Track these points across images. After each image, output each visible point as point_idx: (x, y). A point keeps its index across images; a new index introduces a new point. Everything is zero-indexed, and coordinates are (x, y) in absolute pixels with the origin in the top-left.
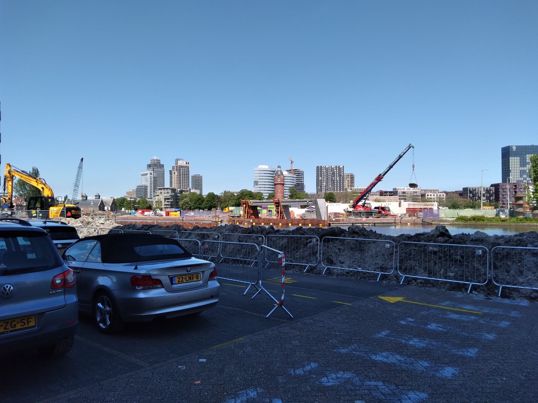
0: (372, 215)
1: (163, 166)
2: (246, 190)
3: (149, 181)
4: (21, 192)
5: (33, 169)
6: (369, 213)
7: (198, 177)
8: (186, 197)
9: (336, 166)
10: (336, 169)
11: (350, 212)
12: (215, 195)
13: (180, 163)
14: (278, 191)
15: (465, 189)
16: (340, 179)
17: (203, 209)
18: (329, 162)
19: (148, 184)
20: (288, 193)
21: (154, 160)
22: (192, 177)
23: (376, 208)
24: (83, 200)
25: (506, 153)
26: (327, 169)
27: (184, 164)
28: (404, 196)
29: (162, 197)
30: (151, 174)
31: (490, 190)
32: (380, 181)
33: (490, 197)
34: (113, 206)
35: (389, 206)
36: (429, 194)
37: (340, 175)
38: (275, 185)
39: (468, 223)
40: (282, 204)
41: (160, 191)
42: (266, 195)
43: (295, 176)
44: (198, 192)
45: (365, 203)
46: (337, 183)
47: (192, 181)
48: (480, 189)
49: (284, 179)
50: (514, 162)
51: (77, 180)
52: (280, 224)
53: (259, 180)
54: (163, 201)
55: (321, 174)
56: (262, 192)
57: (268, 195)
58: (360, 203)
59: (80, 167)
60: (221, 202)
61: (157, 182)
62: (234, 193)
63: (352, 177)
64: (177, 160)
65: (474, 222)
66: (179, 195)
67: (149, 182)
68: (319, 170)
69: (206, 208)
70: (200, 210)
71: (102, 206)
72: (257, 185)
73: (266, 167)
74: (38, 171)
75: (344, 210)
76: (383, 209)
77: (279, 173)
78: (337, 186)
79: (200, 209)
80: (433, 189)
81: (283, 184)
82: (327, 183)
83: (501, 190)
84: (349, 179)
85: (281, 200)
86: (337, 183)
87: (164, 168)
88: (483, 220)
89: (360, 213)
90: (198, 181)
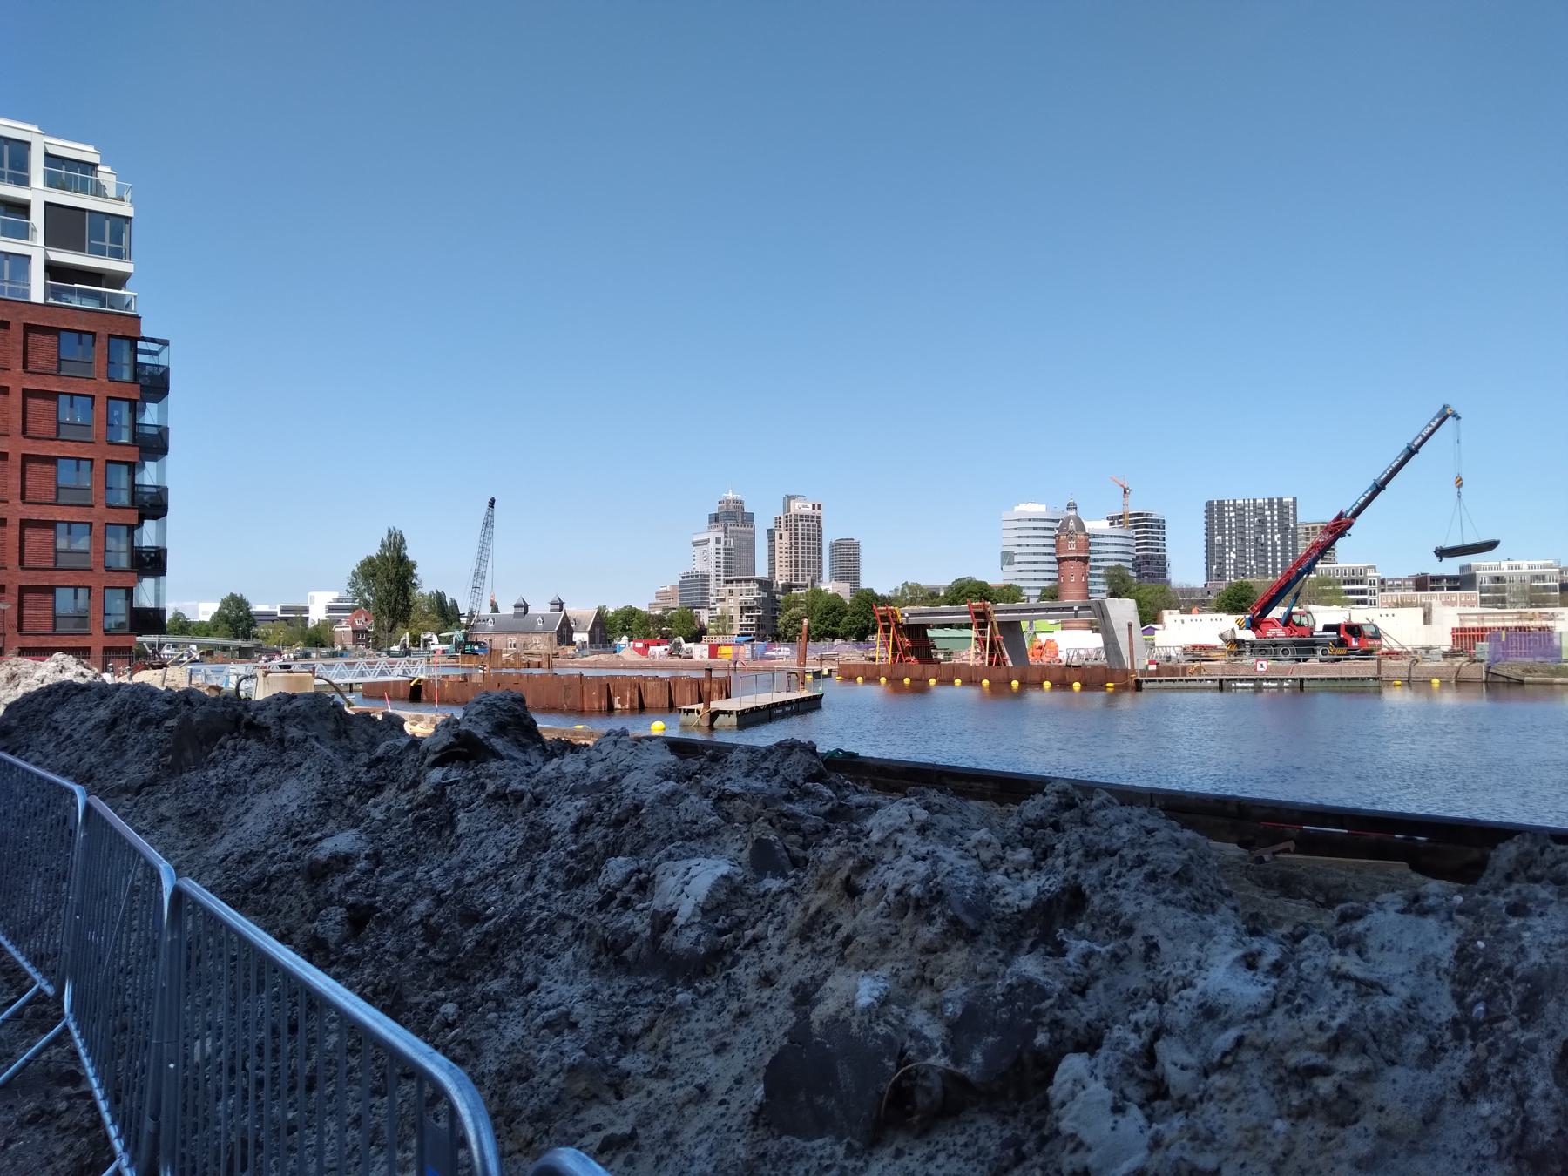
1: (750, 517)
2: (970, 581)
3: (713, 560)
5: (390, 535)
6: (1305, 647)
9: (1271, 501)
10: (1271, 509)
11: (1240, 643)
13: (797, 507)
16: (1284, 540)
17: (844, 638)
18: (1246, 488)
19: (712, 570)
20: (1101, 588)
22: (833, 546)
23: (1327, 628)
24: (516, 615)
26: (1239, 510)
27: (809, 510)
28: (1497, 590)
30: (718, 540)
32: (1342, 534)
34: (598, 630)
35: (1383, 625)
37: (1284, 529)
38: (1060, 561)
40: (996, 617)
42: (1032, 594)
43: (1132, 533)
45: (1290, 615)
46: (1274, 551)
47: (833, 559)
51: (482, 560)
52: (907, 681)
53: (1017, 550)
54: (736, 614)
55: (1221, 523)
56: (1019, 584)
57: (1038, 592)
58: (1278, 612)
59: (488, 524)
61: (735, 564)
62: (938, 589)
64: (788, 499)
68: (1215, 513)
70: (837, 642)
71: (565, 633)
72: (1011, 563)
73: (1038, 509)
74: (403, 541)
75: (1221, 636)
76: (1354, 630)
77: (1072, 524)
79: (834, 636)
81: (1085, 560)
82: (1241, 553)
86: (1274, 551)
87: (756, 522)
89: (1275, 645)
90: (847, 558)
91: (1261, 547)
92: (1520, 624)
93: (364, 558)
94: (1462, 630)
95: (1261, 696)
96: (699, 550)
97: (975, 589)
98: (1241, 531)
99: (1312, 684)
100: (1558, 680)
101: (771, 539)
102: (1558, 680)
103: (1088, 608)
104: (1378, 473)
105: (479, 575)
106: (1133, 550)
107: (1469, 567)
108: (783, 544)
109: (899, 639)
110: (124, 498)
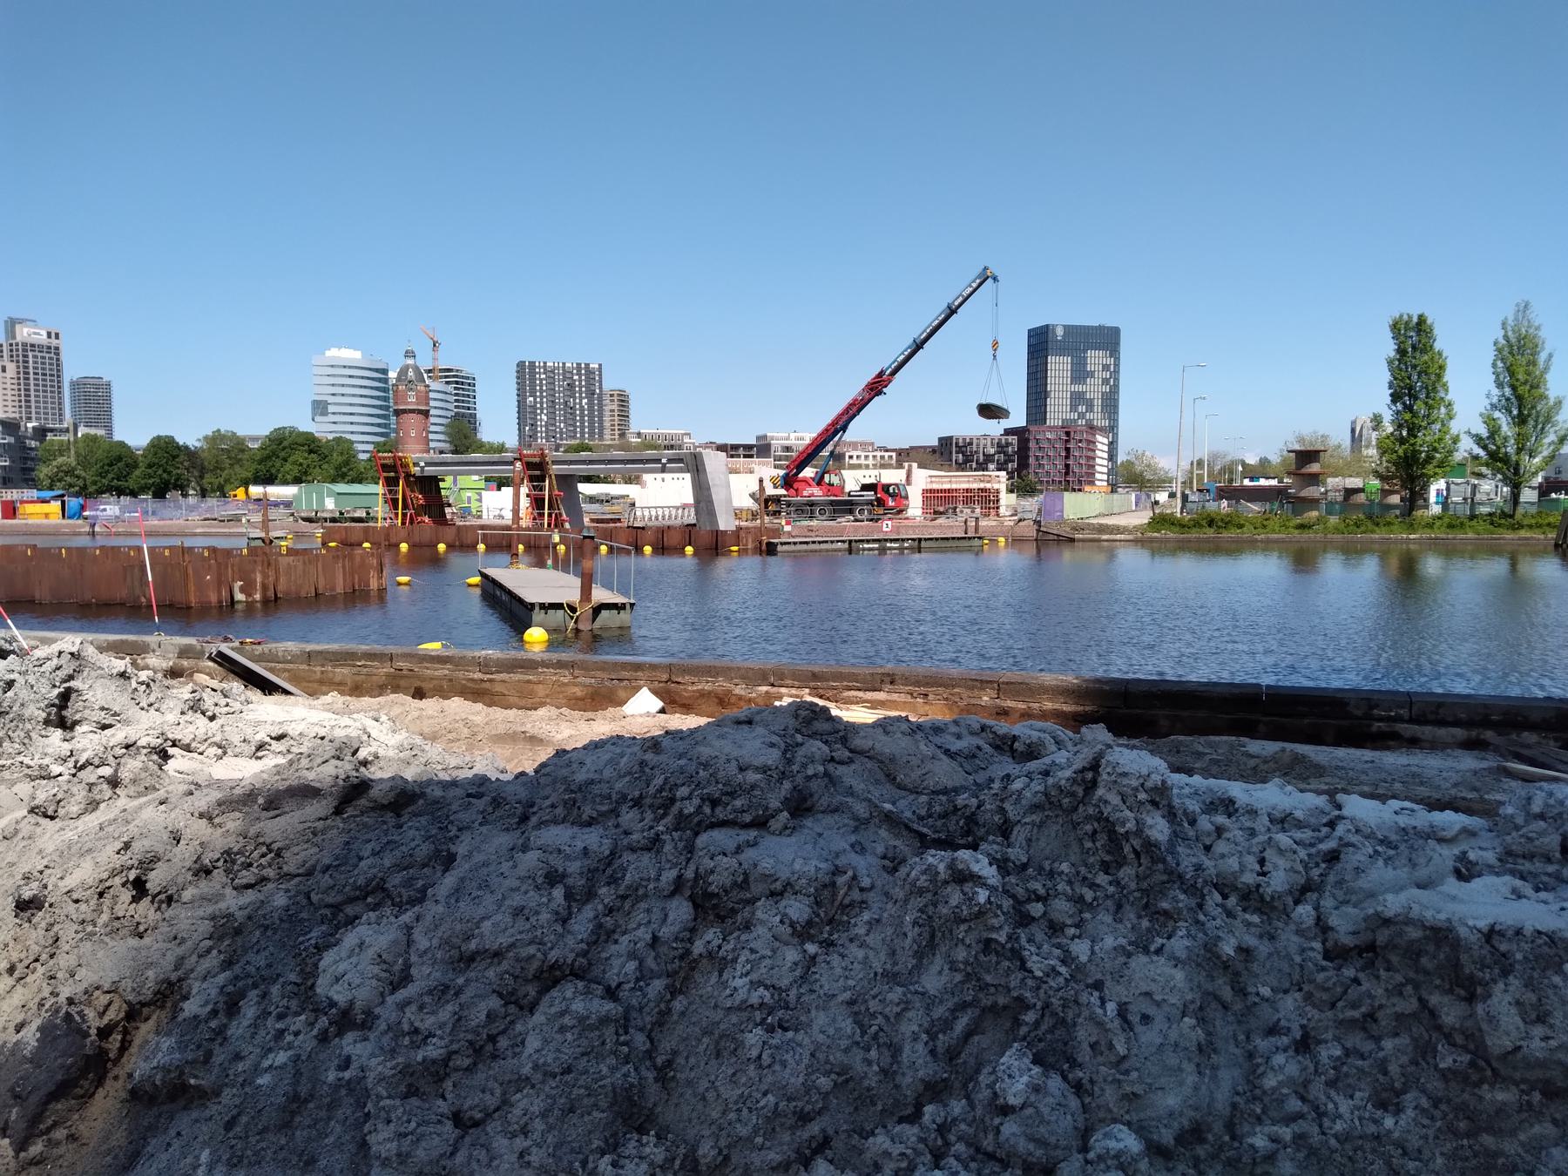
0: (851, 512)
2: (293, 431)
6: (844, 506)
7: (97, 387)
8: (63, 449)
9: (579, 365)
10: (579, 374)
12: (178, 447)
13: (24, 333)
14: (407, 434)
15: (946, 442)
16: (590, 404)
17: (134, 494)
18: (558, 350)
23: (865, 487)
25: (1040, 344)
27: (42, 338)
31: (1008, 444)
32: (880, 393)
33: (1006, 462)
36: (855, 454)
39: (1194, 534)
40: (555, 469)
43: (450, 388)
44: (101, 432)
46: (582, 415)
47: (73, 400)
48: (982, 442)
49: (428, 399)
50: (1058, 367)
52: (404, 547)
53: (331, 399)
60: (203, 471)
63: (623, 400)
64: (11, 324)
65: (1210, 533)
66: (33, 444)
68: (526, 374)
69: (144, 489)
72: (324, 413)
73: (352, 355)
77: (411, 373)
79: (120, 492)
80: (859, 439)
83: (1032, 444)
84: (615, 407)
85: (551, 455)
86: (582, 415)
88: (1241, 526)
89: (812, 504)
90: (95, 398)
91: (570, 410)
92: (982, 485)
94: (931, 491)
95: (888, 556)
97: (300, 440)
99: (785, 548)
100: (1105, 537)
102: (1105, 537)
103: (680, 460)
104: (917, 331)
106: (451, 406)
107: (765, 437)
109: (408, 493)
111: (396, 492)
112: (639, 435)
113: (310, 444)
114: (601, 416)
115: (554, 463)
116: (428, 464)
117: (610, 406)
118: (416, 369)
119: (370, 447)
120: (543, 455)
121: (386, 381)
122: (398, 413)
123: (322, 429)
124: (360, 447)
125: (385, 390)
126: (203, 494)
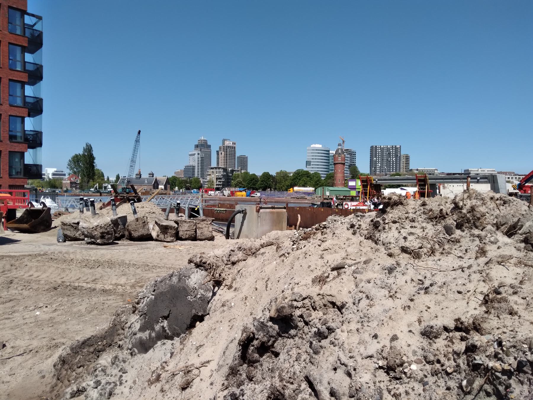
1: (210, 146)
3: (197, 161)
4: (75, 170)
5: (87, 145)
7: (244, 158)
8: (238, 177)
9: (392, 146)
10: (392, 149)
12: (270, 176)
13: (227, 143)
21: (202, 140)
24: (137, 178)
27: (231, 144)
29: (213, 177)
30: (198, 154)
37: (396, 156)
40: (430, 181)
41: (212, 170)
46: (393, 164)
53: (312, 160)
54: (215, 181)
55: (376, 154)
59: (137, 141)
61: (205, 161)
63: (407, 158)
64: (224, 141)
66: (231, 175)
67: (197, 163)
68: (373, 150)
72: (310, 165)
74: (91, 148)
77: (340, 151)
78: (393, 168)
82: (382, 164)
84: (404, 161)
86: (393, 164)
90: (243, 161)
93: (74, 155)
96: (191, 157)
97: (304, 173)
98: (382, 155)
101: (218, 154)
105: (133, 161)
107: (468, 170)
108: (222, 156)
110: (19, 102)
111: (367, 190)
112: (417, 170)
113: (307, 174)
114: (400, 164)
115: (429, 179)
116: (378, 180)
117: (403, 160)
118: (342, 150)
119: (325, 176)
120: (426, 176)
121: (329, 154)
122: (335, 164)
123: (311, 170)
124: (322, 175)
125: (328, 157)
126: (275, 189)
